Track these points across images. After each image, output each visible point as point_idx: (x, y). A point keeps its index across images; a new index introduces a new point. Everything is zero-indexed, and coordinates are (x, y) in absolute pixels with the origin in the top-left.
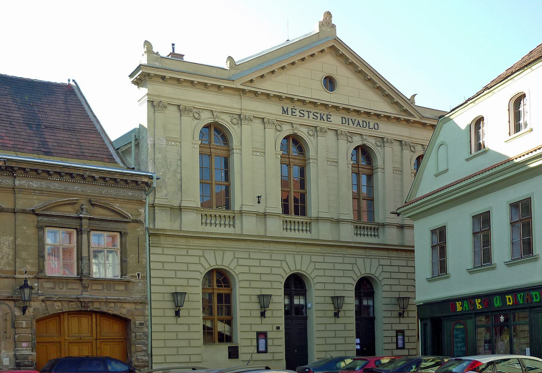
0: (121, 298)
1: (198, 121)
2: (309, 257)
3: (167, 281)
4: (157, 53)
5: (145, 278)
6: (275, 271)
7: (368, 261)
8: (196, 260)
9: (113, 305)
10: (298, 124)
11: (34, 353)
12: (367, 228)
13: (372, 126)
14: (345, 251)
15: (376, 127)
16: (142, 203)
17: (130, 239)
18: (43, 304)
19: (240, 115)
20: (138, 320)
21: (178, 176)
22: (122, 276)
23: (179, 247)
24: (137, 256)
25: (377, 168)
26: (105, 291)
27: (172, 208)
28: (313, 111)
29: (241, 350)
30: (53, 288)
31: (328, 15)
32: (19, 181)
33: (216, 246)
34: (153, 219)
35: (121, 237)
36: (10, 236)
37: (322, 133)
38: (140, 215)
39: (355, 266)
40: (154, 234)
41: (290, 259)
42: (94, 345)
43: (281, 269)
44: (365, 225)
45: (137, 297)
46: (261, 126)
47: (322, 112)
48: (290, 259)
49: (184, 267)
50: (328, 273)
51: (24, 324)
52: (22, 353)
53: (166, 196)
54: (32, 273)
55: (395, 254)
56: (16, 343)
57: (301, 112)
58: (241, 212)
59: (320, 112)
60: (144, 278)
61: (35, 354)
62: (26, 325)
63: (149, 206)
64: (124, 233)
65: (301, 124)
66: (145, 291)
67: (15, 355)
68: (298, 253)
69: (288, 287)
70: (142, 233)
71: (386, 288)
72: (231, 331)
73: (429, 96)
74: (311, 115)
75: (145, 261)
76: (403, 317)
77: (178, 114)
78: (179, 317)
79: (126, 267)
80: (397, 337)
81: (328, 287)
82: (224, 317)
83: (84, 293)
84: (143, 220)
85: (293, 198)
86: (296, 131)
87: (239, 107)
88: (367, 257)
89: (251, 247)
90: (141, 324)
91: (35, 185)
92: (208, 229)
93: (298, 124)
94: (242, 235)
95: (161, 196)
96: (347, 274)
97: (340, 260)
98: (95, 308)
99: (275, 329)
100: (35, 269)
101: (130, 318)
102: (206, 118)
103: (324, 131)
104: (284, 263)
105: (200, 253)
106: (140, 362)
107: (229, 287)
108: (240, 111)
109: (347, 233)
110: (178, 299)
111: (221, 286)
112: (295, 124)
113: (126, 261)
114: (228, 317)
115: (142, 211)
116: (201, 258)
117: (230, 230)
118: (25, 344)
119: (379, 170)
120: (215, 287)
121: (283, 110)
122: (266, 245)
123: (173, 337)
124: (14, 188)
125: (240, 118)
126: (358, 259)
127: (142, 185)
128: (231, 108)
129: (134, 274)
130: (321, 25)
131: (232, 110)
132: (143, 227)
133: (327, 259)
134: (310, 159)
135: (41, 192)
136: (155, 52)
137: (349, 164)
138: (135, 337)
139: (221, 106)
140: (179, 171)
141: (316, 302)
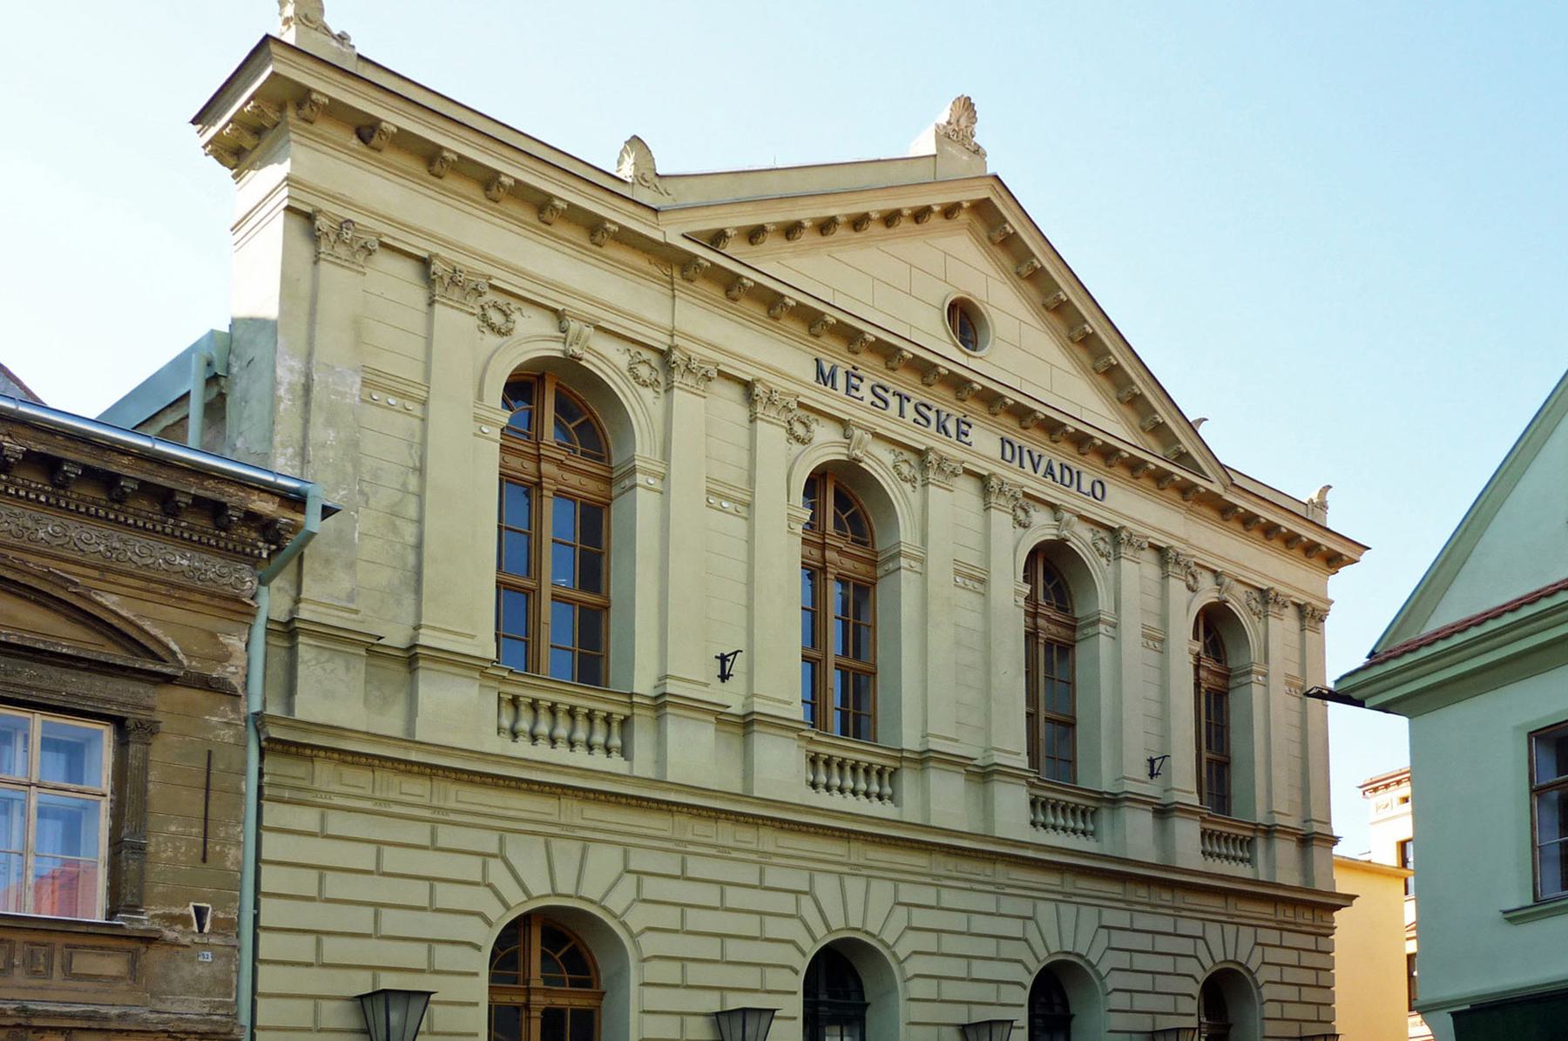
0: (103, 1010)
1: (802, 447)
2: (890, 886)
3: (334, 950)
4: (342, 38)
5: (229, 926)
6: (775, 928)
7: (1068, 911)
8: (470, 868)
10: (866, 429)
13: (1086, 487)
14: (1002, 873)
15: (1098, 492)
16: (240, 609)
17: (164, 757)
19: (664, 355)
21: (409, 533)
22: (111, 914)
23: (396, 809)
24: (197, 830)
25: (1249, 673)
27: (373, 649)
31: (967, 106)
33: (554, 819)
35: (122, 742)
38: (224, 657)
40: (288, 746)
41: (826, 887)
43: (797, 923)
48: (826, 887)
49: (417, 893)
50: (951, 944)
53: (351, 597)
55: (1142, 893)
57: (922, 409)
58: (660, 704)
59: (936, 406)
60: (229, 927)
63: (268, 632)
64: (140, 725)
65: (875, 427)
66: (226, 985)
68: (856, 870)
70: (227, 735)
71: (1119, 1000)
73: (1249, 441)
74: (909, 408)
77: (418, 295)
79: (141, 874)
81: (951, 990)
84: (236, 682)
86: (577, 350)
87: (665, 321)
88: (1067, 898)
89: (689, 837)
93: (866, 429)
94: (746, 797)
95: (326, 592)
96: (1009, 949)
97: (988, 903)
102: (534, 338)
103: (366, 247)
104: (806, 902)
105: (490, 842)
107: (587, 984)
108: (667, 340)
109: (1011, 815)
111: (561, 982)
112: (575, 318)
113: (140, 849)
115: (236, 643)
116: (492, 862)
117: (616, 764)
119: (1102, 628)
120: (537, 981)
121: (820, 371)
122: (746, 836)
125: (1265, 596)
126: (818, 878)
127: (244, 531)
128: (1245, 568)
129: (177, 911)
130: (946, 136)
131: (620, 320)
133: (949, 898)
134: (899, 554)
136: (336, 32)
137: (798, 520)
139: (609, 307)
140: (412, 510)
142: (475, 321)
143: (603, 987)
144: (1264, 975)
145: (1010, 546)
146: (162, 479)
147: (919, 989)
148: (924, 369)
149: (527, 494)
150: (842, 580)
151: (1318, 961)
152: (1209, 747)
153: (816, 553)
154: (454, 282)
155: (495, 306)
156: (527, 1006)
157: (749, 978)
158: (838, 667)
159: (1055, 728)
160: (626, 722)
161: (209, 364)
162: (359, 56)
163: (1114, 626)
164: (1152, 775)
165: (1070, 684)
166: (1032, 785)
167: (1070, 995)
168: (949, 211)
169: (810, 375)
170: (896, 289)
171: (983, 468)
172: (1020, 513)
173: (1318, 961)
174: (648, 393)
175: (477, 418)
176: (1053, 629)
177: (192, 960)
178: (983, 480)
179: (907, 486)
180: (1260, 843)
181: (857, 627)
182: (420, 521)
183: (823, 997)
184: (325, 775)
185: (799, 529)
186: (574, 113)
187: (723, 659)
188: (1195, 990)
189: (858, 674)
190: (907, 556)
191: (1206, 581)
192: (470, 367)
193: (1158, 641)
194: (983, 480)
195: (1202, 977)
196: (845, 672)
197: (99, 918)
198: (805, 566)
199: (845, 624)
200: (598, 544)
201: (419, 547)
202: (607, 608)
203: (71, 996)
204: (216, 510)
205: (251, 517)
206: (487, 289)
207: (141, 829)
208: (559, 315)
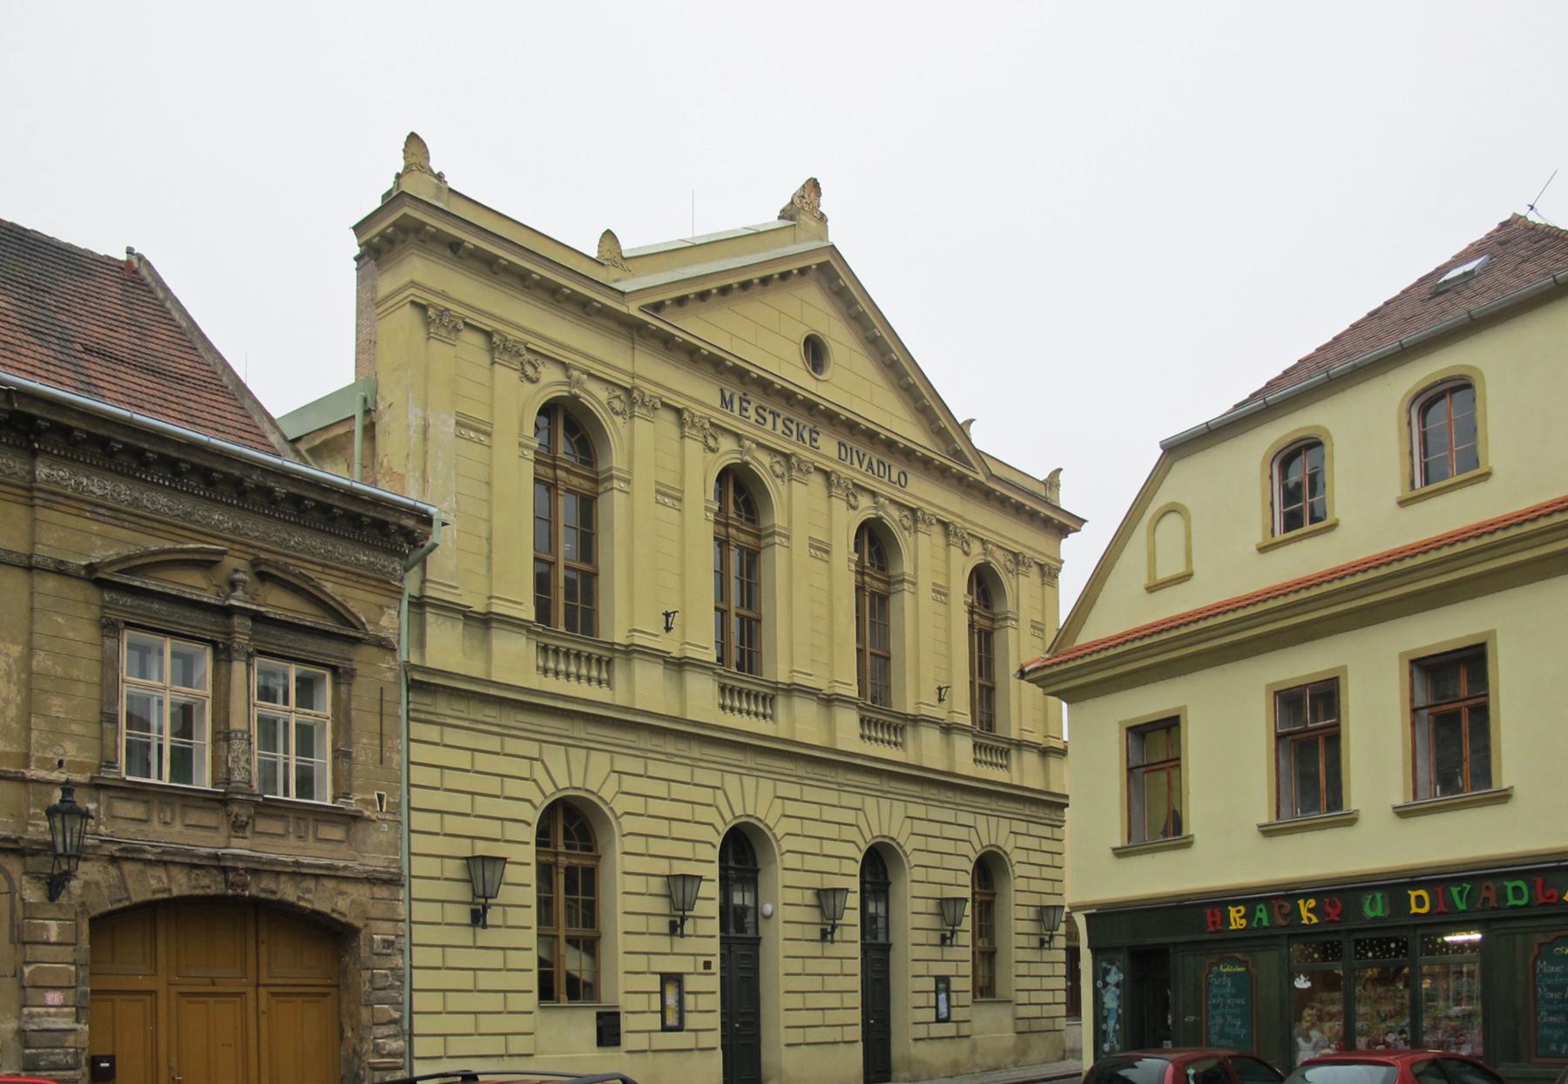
0: (336, 863)
6: (513, 788)
9: (311, 884)
11: (84, 1027)
12: (589, 658)
13: (894, 477)
18: (113, 871)
20: (381, 932)
22: (335, 799)
23: (481, 727)
24: (377, 742)
26: (292, 840)
28: (784, 414)
29: (627, 1023)
30: (145, 821)
32: (50, 467)
34: (421, 643)
35: (336, 684)
36: (14, 642)
37: (506, 358)
39: (537, 765)
40: (426, 686)
42: (252, 1005)
44: (582, 648)
45: (375, 862)
46: (674, 432)
47: (803, 422)
51: (53, 931)
52: (46, 1026)
54: (80, 767)
56: (26, 992)
61: (86, 1028)
62: (59, 934)
66: (397, 849)
67: (21, 1032)
69: (546, 845)
70: (390, 676)
72: (596, 973)
73: (1006, 437)
74: (779, 422)
75: (397, 759)
76: (682, 935)
78: (485, 926)
80: (663, 993)
82: (579, 931)
83: (234, 841)
85: (562, 583)
88: (884, 795)
90: (389, 944)
91: (95, 489)
92: (552, 684)
98: (263, 890)
99: (701, 968)
100: (90, 757)
101: (359, 924)
105: (531, 749)
106: (383, 1056)
107: (590, 849)
110: (482, 874)
112: (576, 368)
113: (348, 755)
114: (588, 932)
118: (54, 997)
120: (562, 849)
121: (723, 397)
123: (462, 986)
124: (30, 489)
126: (728, 777)
129: (368, 797)
132: (394, 659)
135: (115, 514)
138: (371, 981)
141: (784, 900)
142: (518, 374)
143: (600, 852)
144: (1016, 856)
145: (845, 523)
146: (355, 508)
147: (791, 861)
148: (788, 397)
149: (548, 490)
150: (741, 549)
151: (1053, 846)
152: (980, 675)
153: (722, 530)
154: (505, 348)
155: (530, 362)
156: (556, 864)
157: (493, 829)
158: (737, 615)
159: (877, 662)
160: (609, 662)
161: (365, 400)
162: (451, 190)
163: (914, 584)
164: (940, 700)
165: (886, 626)
166: (860, 708)
167: (758, 857)
168: (803, 271)
169: (717, 403)
170: (765, 339)
171: (828, 466)
172: (851, 499)
173: (1053, 846)
174: (619, 420)
175: (521, 445)
176: (875, 584)
177: (377, 830)
178: (827, 475)
179: (779, 481)
180: (1014, 753)
181: (749, 584)
182: (489, 521)
183: (732, 864)
184: (443, 706)
185: (711, 516)
186: (569, 220)
187: (667, 615)
188: (970, 867)
189: (750, 620)
190: (780, 534)
191: (976, 548)
192: (516, 403)
193: (941, 592)
194: (827, 475)
195: (974, 857)
196: (742, 618)
197: (329, 803)
198: (716, 539)
199: (742, 582)
200: (590, 527)
201: (489, 539)
202: (596, 575)
203: (318, 853)
204: (382, 526)
205: (401, 527)
206: (524, 352)
207: (349, 743)
208: (565, 367)
